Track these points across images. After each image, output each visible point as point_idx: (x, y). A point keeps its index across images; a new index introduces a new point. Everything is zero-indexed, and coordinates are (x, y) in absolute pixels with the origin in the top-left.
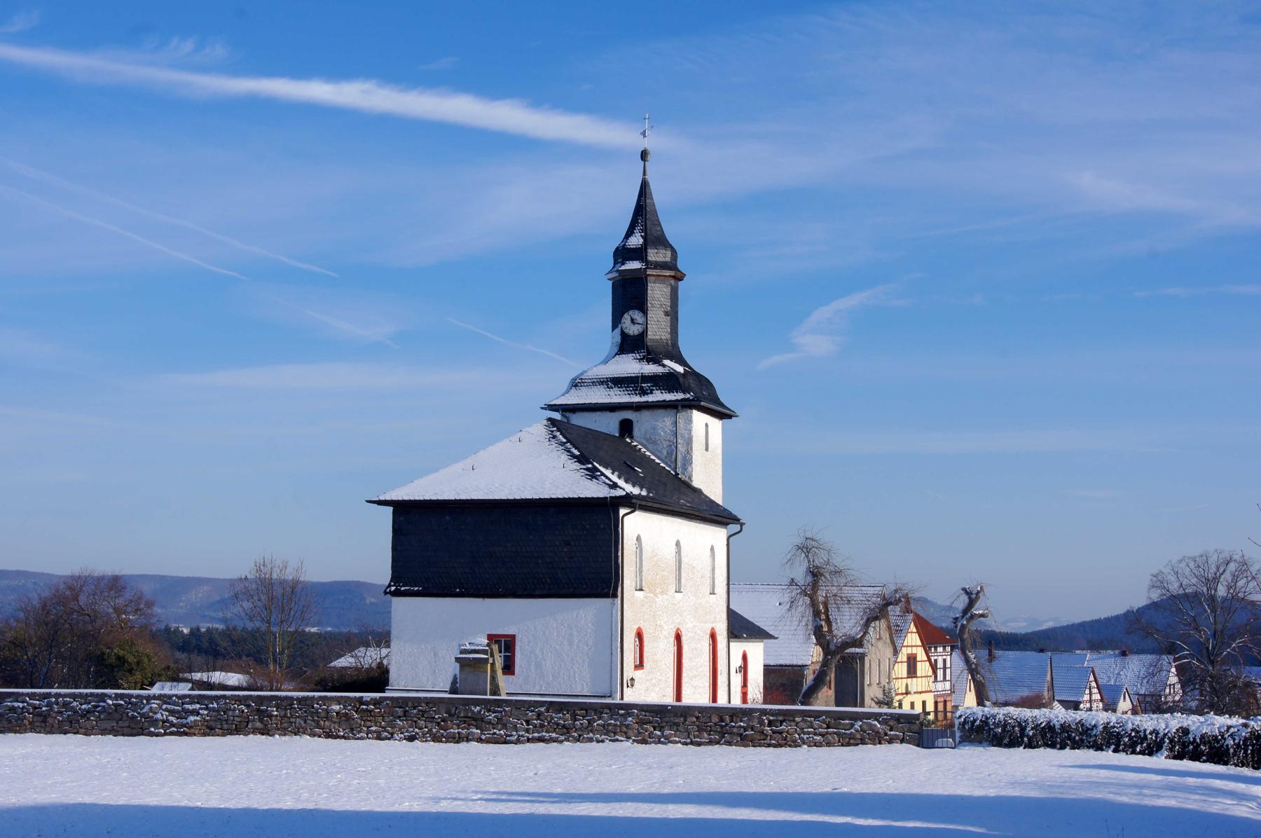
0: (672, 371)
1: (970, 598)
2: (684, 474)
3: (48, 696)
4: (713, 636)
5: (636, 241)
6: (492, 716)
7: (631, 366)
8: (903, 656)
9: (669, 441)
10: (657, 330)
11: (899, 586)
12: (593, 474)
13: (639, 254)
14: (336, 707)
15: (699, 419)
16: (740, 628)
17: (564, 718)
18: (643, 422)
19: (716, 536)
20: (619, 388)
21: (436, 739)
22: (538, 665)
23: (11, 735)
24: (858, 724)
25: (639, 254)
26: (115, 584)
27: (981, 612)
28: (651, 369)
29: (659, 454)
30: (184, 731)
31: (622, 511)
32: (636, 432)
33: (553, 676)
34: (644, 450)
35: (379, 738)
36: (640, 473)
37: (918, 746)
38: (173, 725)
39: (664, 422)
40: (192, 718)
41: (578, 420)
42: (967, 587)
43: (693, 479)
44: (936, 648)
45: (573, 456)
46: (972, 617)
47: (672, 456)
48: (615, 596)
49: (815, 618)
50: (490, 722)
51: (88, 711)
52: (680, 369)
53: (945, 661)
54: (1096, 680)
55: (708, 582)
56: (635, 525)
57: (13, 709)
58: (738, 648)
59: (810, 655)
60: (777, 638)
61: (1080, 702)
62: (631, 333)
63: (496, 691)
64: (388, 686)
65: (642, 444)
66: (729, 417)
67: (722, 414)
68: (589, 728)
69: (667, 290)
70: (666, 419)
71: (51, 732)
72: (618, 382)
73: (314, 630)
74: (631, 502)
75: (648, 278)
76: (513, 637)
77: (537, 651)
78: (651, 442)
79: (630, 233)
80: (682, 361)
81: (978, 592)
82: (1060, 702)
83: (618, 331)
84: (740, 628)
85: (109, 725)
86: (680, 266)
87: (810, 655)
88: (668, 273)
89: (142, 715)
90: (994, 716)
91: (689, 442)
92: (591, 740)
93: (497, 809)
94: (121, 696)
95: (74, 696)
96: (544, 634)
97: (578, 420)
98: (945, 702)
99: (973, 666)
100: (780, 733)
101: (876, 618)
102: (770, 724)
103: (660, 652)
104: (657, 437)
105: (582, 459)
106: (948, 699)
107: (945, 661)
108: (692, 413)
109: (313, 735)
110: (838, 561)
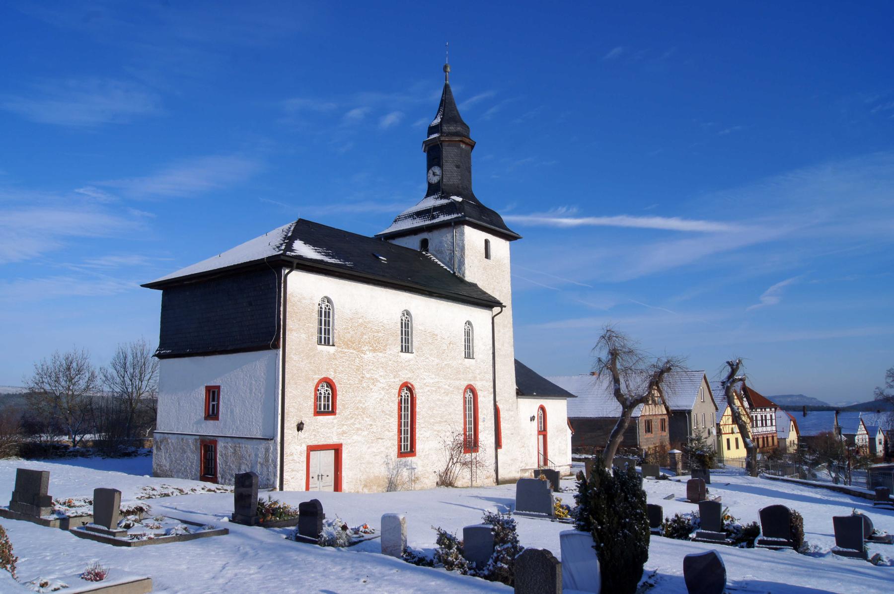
0: (453, 201)
1: (732, 368)
2: (459, 273)
9: (450, 250)
11: (670, 358)
18: (434, 238)
20: (419, 218)
22: (232, 412)
27: (740, 377)
29: (444, 261)
32: (430, 246)
33: (240, 421)
34: (434, 258)
36: (384, 260)
42: (730, 361)
43: (465, 276)
44: (765, 409)
47: (451, 263)
48: (276, 347)
49: (615, 384)
53: (771, 416)
54: (863, 424)
60: (577, 397)
61: (855, 435)
62: (433, 182)
64: (155, 430)
65: (433, 255)
70: (448, 235)
72: (419, 214)
75: (443, 143)
76: (218, 387)
77: (232, 400)
78: (439, 253)
81: (738, 364)
82: (843, 435)
86: (473, 136)
96: (236, 383)
98: (773, 437)
99: (737, 414)
104: (443, 249)
106: (774, 435)
107: (771, 416)
108: (464, 228)
110: (630, 345)
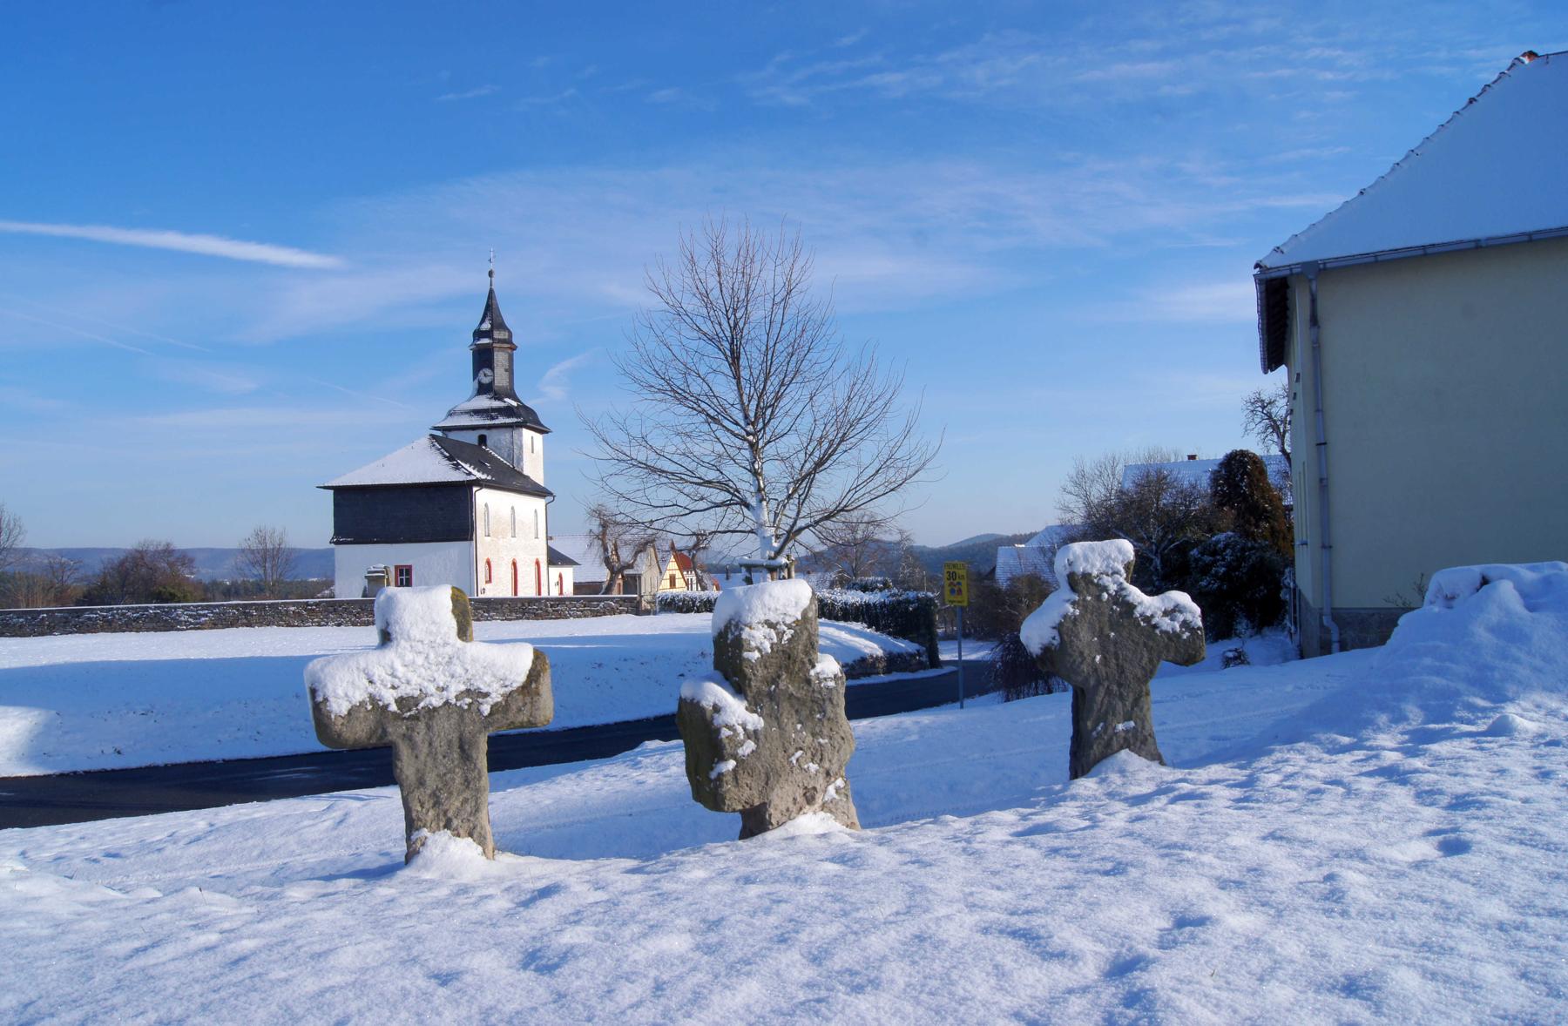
4: (538, 563)
5: (486, 326)
7: (485, 402)
8: (667, 576)
10: (501, 380)
12: (457, 467)
13: (488, 334)
14: (293, 608)
15: (527, 434)
16: (555, 558)
18: (492, 437)
19: (539, 504)
21: (354, 624)
23: (89, 634)
25: (488, 334)
26: (168, 552)
28: (497, 404)
30: (199, 627)
31: (475, 489)
32: (488, 442)
35: (319, 625)
38: (191, 624)
39: (505, 436)
40: (203, 619)
41: (453, 436)
45: (445, 457)
46: (699, 549)
47: (510, 457)
48: (471, 539)
51: (138, 618)
52: (514, 404)
55: (533, 530)
56: (482, 497)
57: (89, 619)
58: (555, 572)
59: (603, 575)
66: (547, 432)
67: (542, 431)
69: (507, 356)
71: (114, 631)
72: (477, 412)
73: (315, 580)
74: (479, 483)
76: (410, 566)
78: (497, 449)
79: (483, 321)
80: (516, 399)
83: (476, 381)
84: (555, 558)
85: (151, 625)
86: (515, 341)
87: (603, 575)
88: (506, 346)
89: (172, 619)
91: (521, 447)
95: (128, 609)
97: (453, 436)
101: (641, 551)
103: (503, 574)
105: (450, 459)
109: (279, 625)
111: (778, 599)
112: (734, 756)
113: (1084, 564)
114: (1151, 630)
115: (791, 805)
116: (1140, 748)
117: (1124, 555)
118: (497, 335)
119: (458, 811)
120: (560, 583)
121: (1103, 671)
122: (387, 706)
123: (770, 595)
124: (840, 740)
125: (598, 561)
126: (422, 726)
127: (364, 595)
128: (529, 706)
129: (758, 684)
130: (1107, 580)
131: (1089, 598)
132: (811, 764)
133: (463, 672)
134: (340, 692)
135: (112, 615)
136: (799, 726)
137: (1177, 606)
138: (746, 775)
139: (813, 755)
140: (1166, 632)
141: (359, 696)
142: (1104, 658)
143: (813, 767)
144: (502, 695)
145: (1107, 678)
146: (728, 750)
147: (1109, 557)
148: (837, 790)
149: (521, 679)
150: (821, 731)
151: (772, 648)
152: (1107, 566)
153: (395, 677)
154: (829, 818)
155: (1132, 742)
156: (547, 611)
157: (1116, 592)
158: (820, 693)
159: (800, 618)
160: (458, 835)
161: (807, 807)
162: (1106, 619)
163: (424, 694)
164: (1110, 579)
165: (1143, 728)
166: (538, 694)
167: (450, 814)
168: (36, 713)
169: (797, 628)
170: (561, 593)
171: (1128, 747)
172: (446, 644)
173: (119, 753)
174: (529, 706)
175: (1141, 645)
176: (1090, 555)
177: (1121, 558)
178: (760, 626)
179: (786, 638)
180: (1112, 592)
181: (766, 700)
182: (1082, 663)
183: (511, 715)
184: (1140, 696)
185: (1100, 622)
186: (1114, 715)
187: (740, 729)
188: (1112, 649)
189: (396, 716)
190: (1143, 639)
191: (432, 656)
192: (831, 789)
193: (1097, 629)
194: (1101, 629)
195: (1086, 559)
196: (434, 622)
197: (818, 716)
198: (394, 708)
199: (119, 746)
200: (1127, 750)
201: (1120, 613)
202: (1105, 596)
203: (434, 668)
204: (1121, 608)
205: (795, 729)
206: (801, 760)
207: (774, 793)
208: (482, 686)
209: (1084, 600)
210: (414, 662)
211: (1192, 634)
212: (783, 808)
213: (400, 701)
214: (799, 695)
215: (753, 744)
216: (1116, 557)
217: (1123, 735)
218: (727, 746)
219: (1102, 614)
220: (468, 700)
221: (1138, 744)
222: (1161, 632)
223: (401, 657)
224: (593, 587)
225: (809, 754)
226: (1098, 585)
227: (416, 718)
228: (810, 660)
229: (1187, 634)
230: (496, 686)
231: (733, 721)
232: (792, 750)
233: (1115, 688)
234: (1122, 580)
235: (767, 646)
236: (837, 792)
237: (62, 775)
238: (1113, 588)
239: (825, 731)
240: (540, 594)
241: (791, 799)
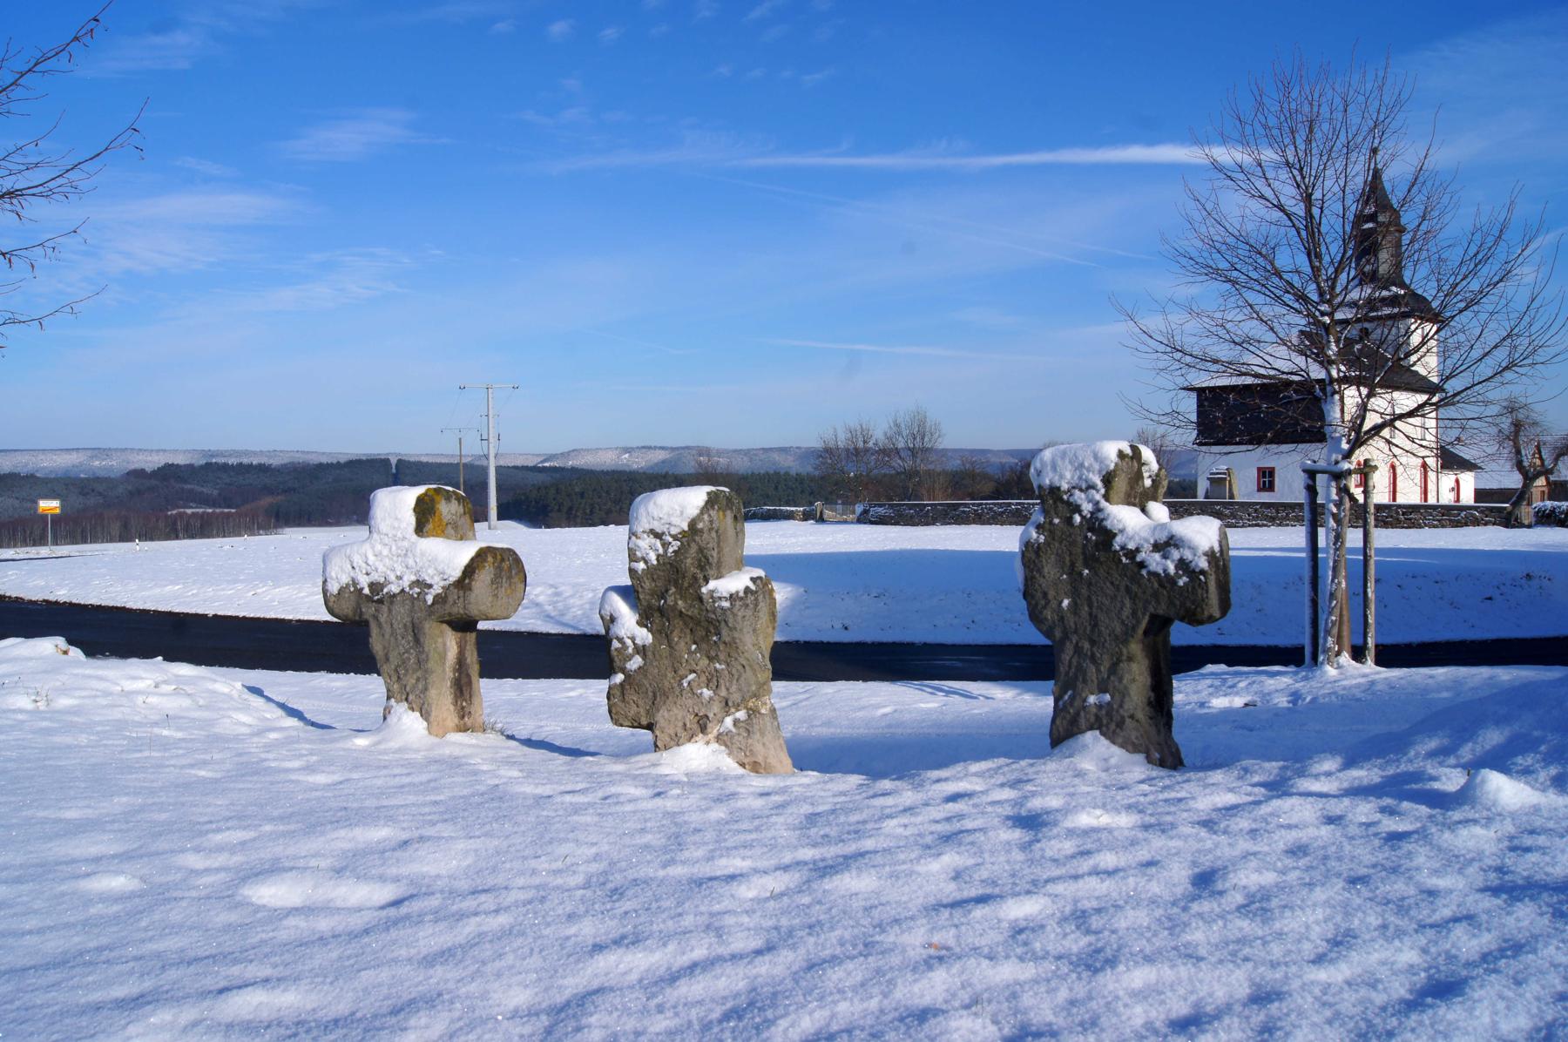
3: (982, 504)
5: (1370, 210)
6: (1227, 512)
17: (1271, 512)
24: (1463, 514)
37: (1507, 527)
50: (1226, 515)
57: (964, 512)
58: (1448, 480)
59: (1514, 481)
63: (1232, 496)
68: (1287, 518)
76: (1274, 468)
85: (1011, 519)
90: (1560, 507)
92: (1287, 525)
93: (227, 547)
94: (1019, 504)
95: (995, 504)
100: (1410, 519)
102: (1404, 514)
111: (662, 507)
112: (623, 670)
113: (1051, 475)
114: (1136, 570)
115: (680, 730)
116: (1114, 732)
117: (1101, 462)
118: (1381, 218)
119: (414, 687)
120: (1457, 488)
121: (1071, 621)
122: (362, 589)
123: (655, 503)
124: (740, 668)
125: (1508, 466)
126: (385, 608)
127: (1206, 497)
128: (462, 599)
129: (647, 597)
130: (1079, 497)
131: (1056, 521)
132: (705, 690)
133: (414, 564)
134: (333, 574)
135: (982, 509)
136: (694, 647)
137: (1172, 537)
138: (632, 691)
139: (709, 681)
140: (1156, 574)
141: (345, 580)
142: (1074, 606)
143: (707, 693)
144: (443, 588)
145: (1076, 632)
146: (617, 663)
147: (1082, 465)
148: (736, 722)
149: (456, 573)
150: (717, 655)
151: (658, 560)
152: (1080, 478)
153: (368, 565)
154: (723, 751)
155: (1105, 722)
156: (1398, 519)
157: (1092, 513)
158: (714, 613)
159: (686, 529)
160: (413, 710)
161: (701, 735)
162: (1079, 550)
163: (387, 582)
164: (1083, 495)
165: (1121, 706)
166: (470, 589)
167: (408, 689)
168: (789, 589)
169: (684, 540)
170: (1458, 500)
171: (1099, 728)
172: (404, 538)
173: (846, 628)
174: (462, 599)
175: (1122, 589)
176: (1059, 462)
177: (1096, 466)
178: (645, 536)
179: (671, 550)
180: (1085, 513)
181: (657, 615)
182: (1045, 607)
183: (447, 606)
184: (1119, 661)
185: (1071, 554)
186: (1085, 681)
187: (629, 642)
188: (1084, 591)
189: (369, 599)
190: (1126, 581)
191: (394, 548)
192: (729, 721)
193: (1068, 563)
194: (1073, 564)
195: (1054, 468)
196: (396, 519)
197: (715, 638)
198: (366, 591)
199: (847, 622)
200: (1097, 732)
201: (1097, 544)
202: (1077, 518)
203: (395, 558)
204: (1097, 536)
205: (689, 649)
206: (694, 685)
207: (660, 714)
208: (427, 578)
209: (1051, 523)
210: (381, 553)
211: (1191, 580)
212: (672, 732)
213: (372, 585)
214: (690, 613)
215: (640, 660)
216: (1091, 465)
217: (1094, 710)
218: (616, 659)
219: (1073, 543)
220: (417, 590)
221: (1113, 726)
222: (1149, 573)
223: (373, 547)
224: (1502, 495)
225: (703, 678)
226: (1068, 503)
227: (380, 601)
228: (705, 576)
229: (1185, 579)
230: (437, 579)
231: (622, 633)
232: (681, 672)
233: (1087, 645)
234: (1098, 497)
235: (653, 557)
236: (735, 725)
237: (787, 643)
238: (1087, 508)
239: (722, 657)
240: (1426, 500)
241: (681, 724)
